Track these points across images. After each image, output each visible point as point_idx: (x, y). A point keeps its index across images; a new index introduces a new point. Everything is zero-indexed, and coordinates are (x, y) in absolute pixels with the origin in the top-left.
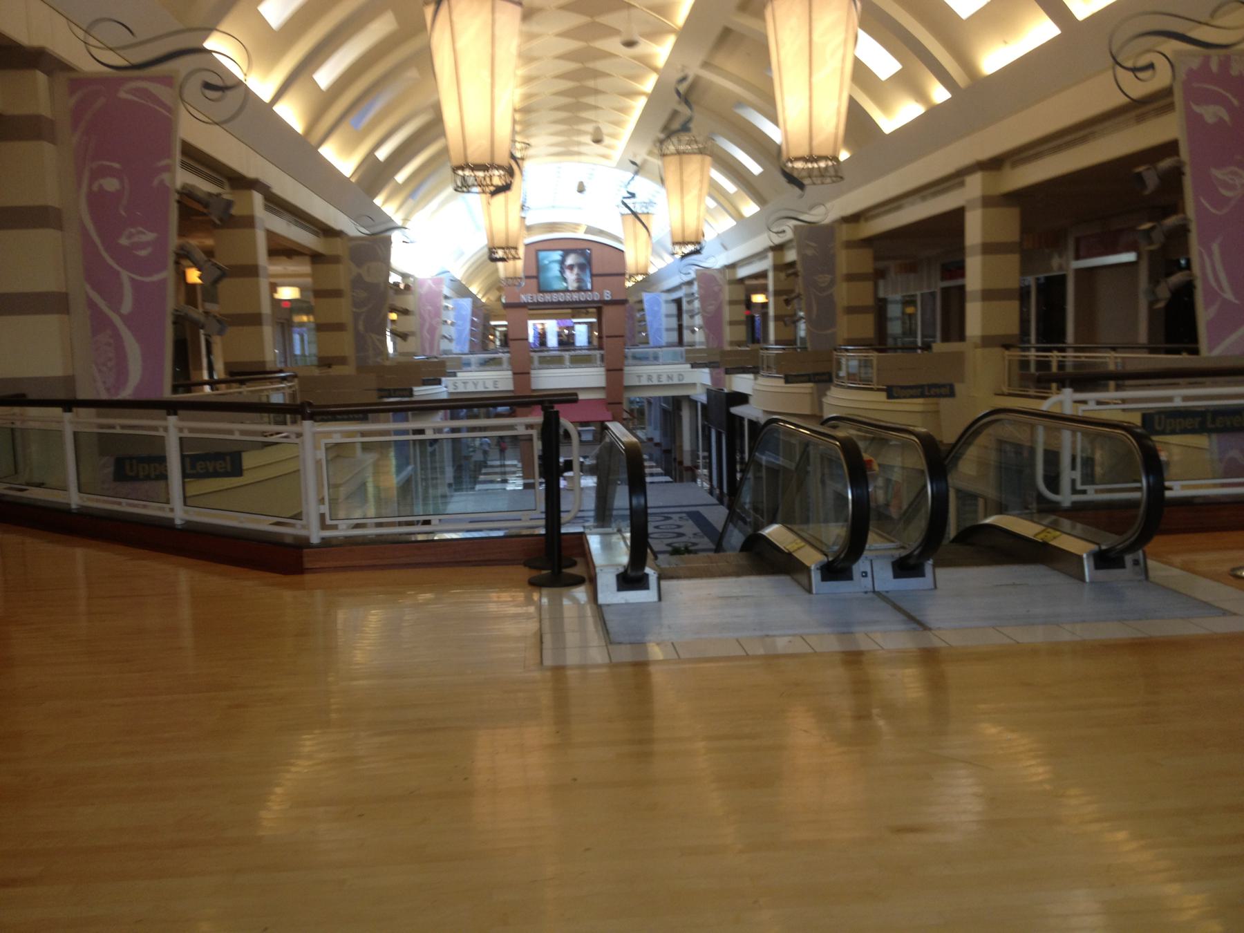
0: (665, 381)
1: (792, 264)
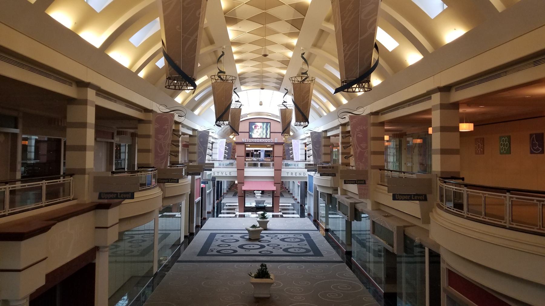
0: (298, 176)
1: (349, 132)
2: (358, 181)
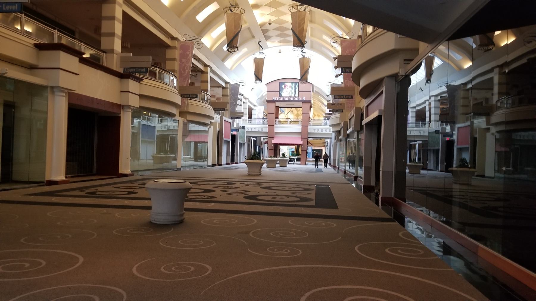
2: (346, 96)
